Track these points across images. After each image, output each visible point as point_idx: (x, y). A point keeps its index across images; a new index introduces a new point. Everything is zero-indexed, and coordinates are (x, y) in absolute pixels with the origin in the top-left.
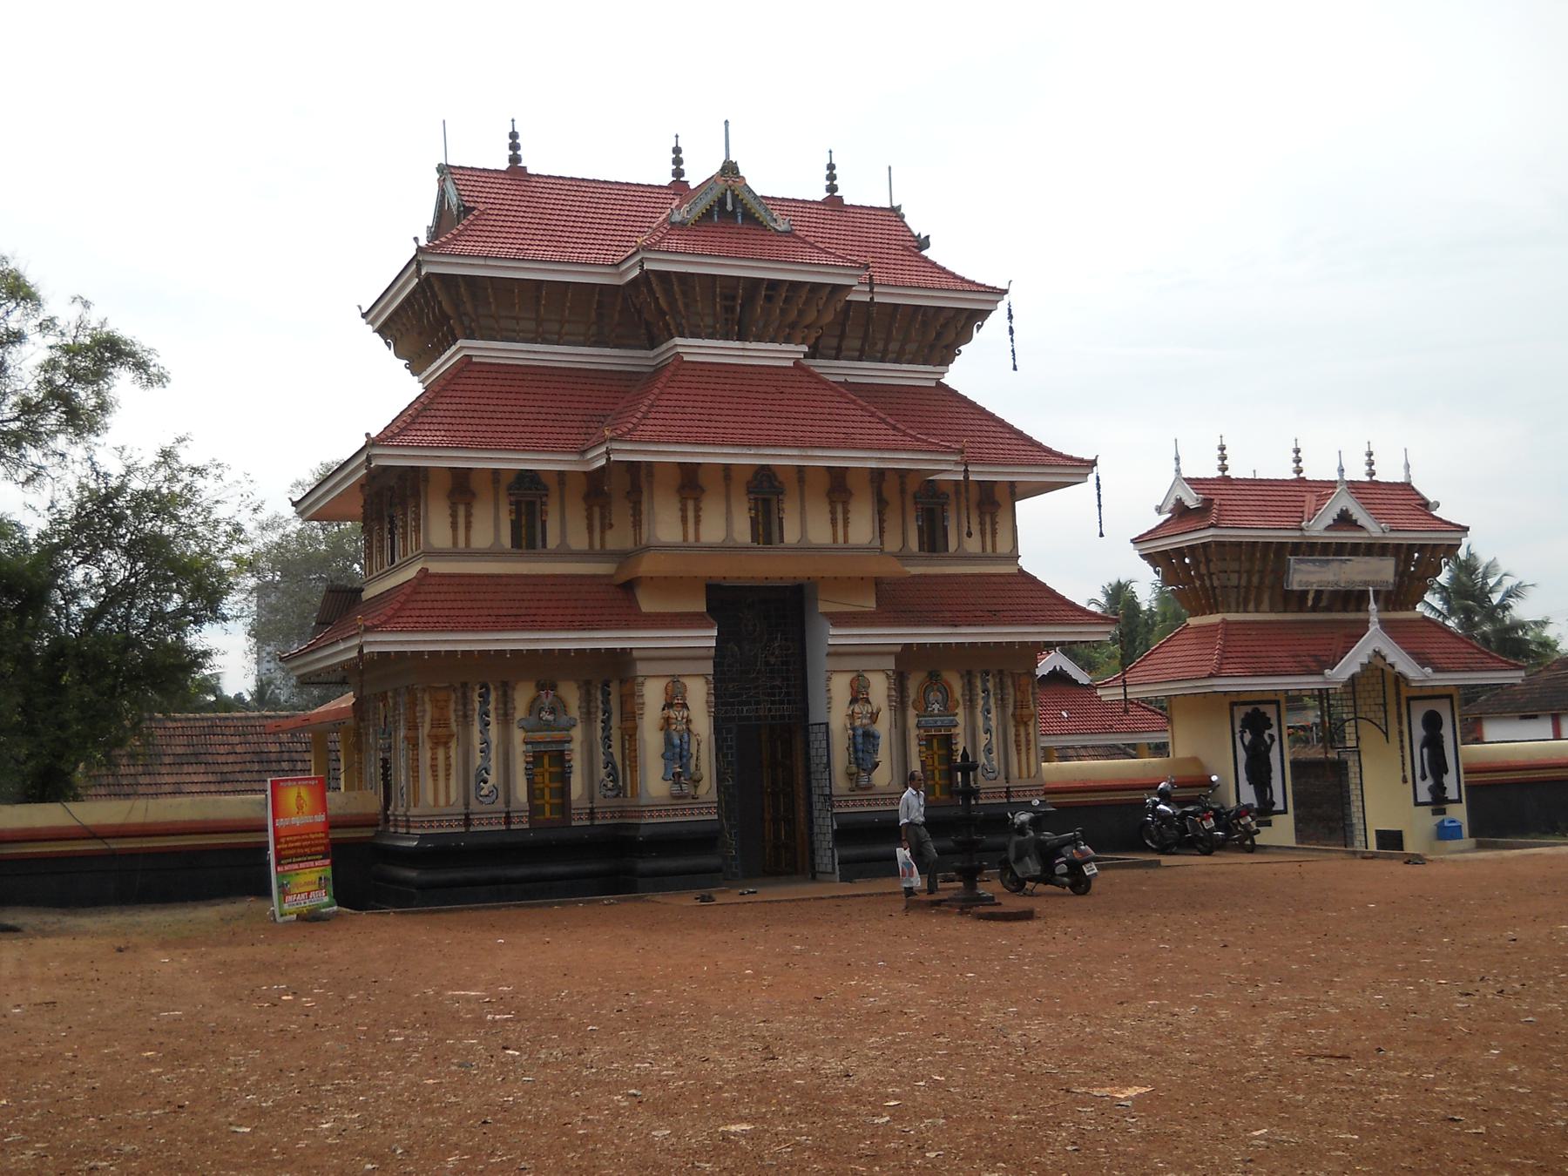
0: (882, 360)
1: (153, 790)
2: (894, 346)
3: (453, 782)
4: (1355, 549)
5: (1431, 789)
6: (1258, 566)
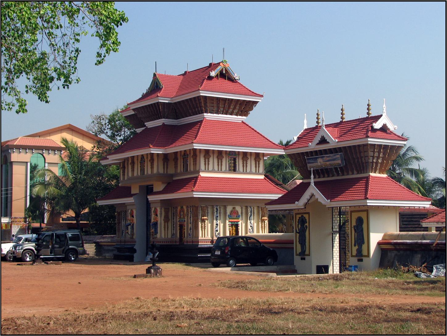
0: (226, 114)
1: (404, 217)
2: (231, 110)
3: (266, 230)
4: (326, 152)
5: (357, 250)
6: (381, 155)
